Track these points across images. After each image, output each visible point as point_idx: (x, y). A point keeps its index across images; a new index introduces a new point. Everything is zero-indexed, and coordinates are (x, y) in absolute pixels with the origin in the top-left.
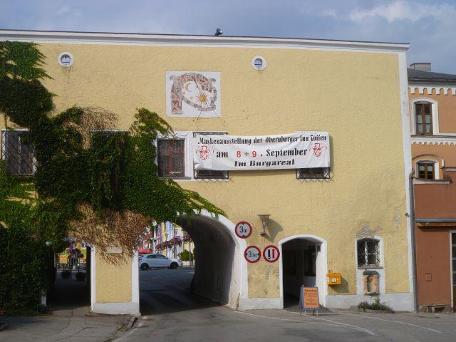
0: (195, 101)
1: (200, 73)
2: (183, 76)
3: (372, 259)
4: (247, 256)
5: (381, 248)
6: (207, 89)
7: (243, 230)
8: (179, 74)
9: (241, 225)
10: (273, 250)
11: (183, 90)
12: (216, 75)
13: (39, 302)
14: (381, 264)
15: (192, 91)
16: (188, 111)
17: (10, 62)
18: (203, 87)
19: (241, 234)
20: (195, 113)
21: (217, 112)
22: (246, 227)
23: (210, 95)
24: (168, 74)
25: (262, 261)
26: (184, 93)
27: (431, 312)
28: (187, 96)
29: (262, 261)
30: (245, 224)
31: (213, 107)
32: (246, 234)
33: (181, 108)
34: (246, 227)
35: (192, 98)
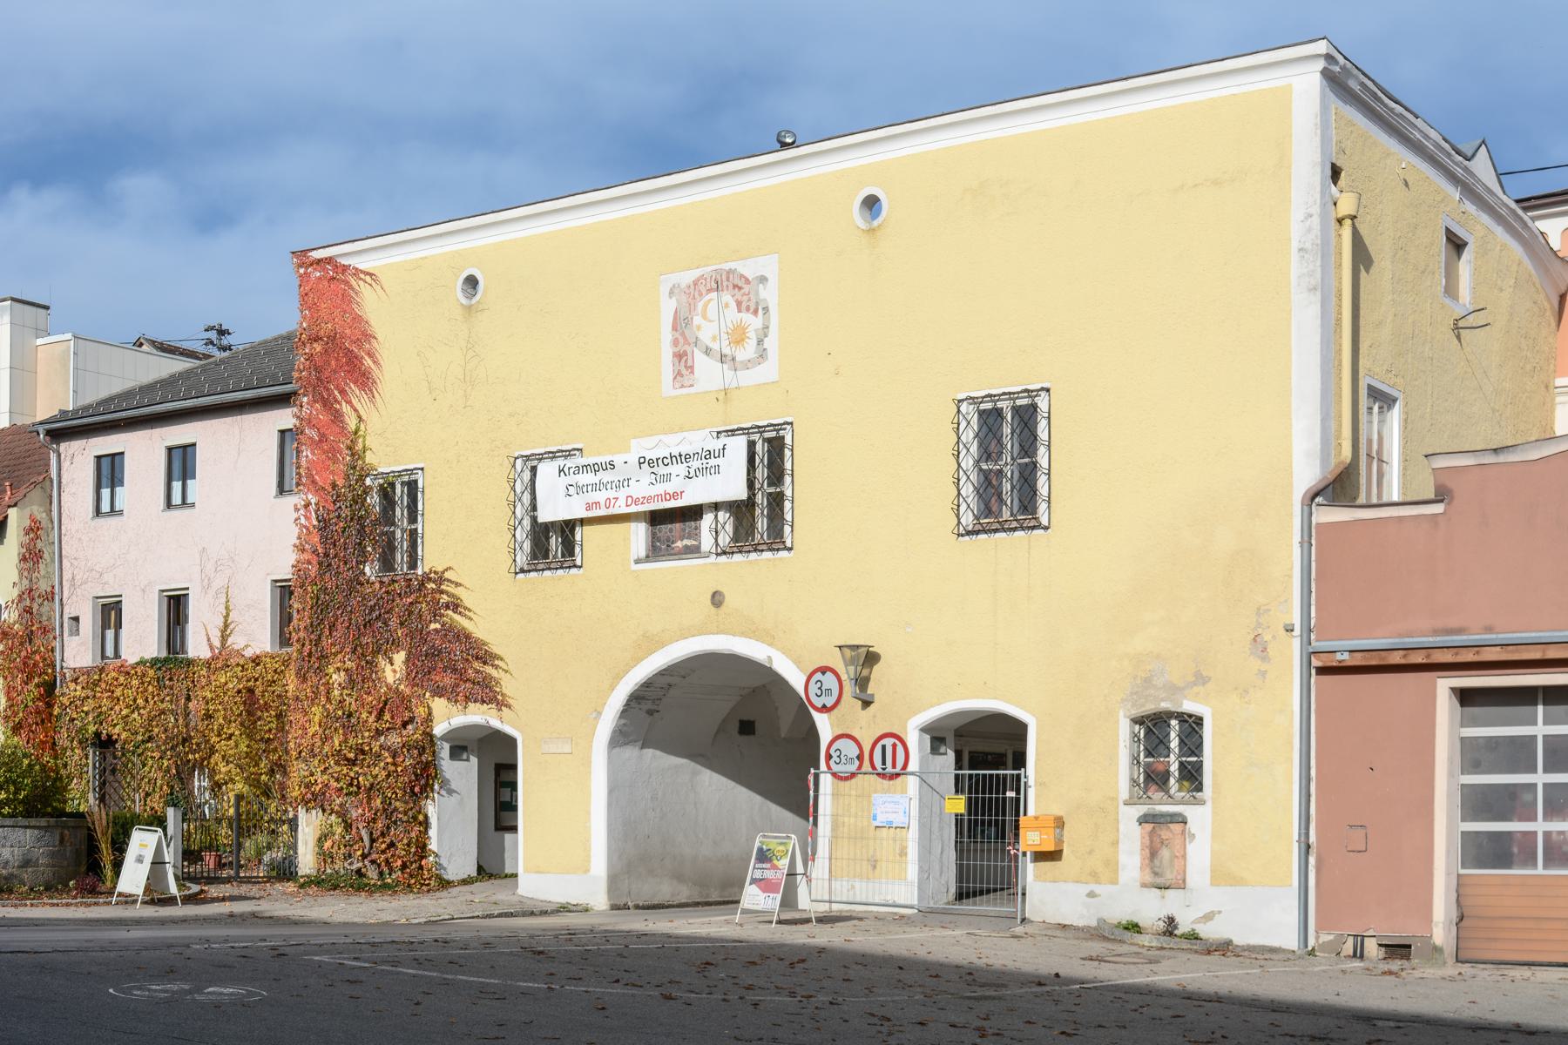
6: (748, 309)
7: (822, 692)
8: (688, 277)
9: (818, 676)
10: (894, 746)
16: (708, 373)
18: (739, 304)
21: (767, 372)
23: (754, 323)
31: (762, 355)
32: (829, 702)
33: (691, 369)
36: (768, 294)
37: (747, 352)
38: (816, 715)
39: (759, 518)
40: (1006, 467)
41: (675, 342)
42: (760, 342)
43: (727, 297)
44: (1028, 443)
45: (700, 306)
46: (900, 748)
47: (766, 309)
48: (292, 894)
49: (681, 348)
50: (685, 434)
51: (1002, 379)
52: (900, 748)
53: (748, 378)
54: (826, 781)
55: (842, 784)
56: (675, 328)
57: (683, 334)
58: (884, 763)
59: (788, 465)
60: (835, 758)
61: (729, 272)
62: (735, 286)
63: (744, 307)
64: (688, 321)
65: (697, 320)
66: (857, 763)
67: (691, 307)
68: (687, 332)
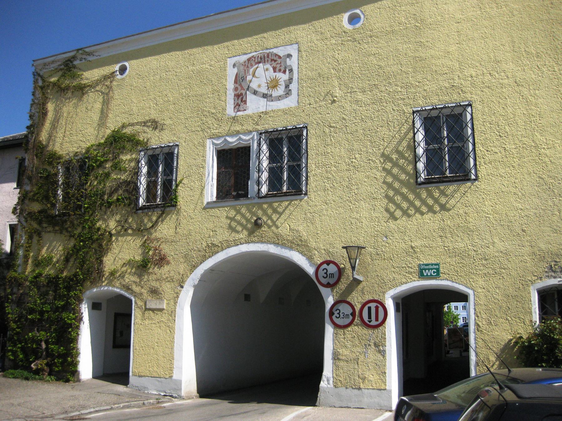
1: (271, 51)
6: (280, 71)
9: (325, 266)
10: (377, 308)
15: (261, 76)
16: (255, 105)
18: (275, 70)
21: (290, 102)
23: (283, 77)
24: (230, 62)
28: (254, 85)
31: (288, 93)
32: (332, 281)
34: (332, 269)
36: (293, 62)
37: (281, 91)
38: (323, 290)
39: (290, 178)
40: (445, 148)
41: (236, 89)
42: (287, 86)
43: (268, 66)
44: (169, 168)
45: (251, 70)
46: (381, 309)
47: (291, 71)
49: (239, 92)
52: (381, 309)
54: (329, 330)
55: (341, 331)
56: (236, 82)
57: (240, 85)
58: (370, 317)
59: (175, 165)
61: (268, 55)
62: (272, 60)
63: (277, 69)
64: (244, 79)
65: (249, 78)
66: (351, 318)
67: (246, 72)
68: (243, 84)
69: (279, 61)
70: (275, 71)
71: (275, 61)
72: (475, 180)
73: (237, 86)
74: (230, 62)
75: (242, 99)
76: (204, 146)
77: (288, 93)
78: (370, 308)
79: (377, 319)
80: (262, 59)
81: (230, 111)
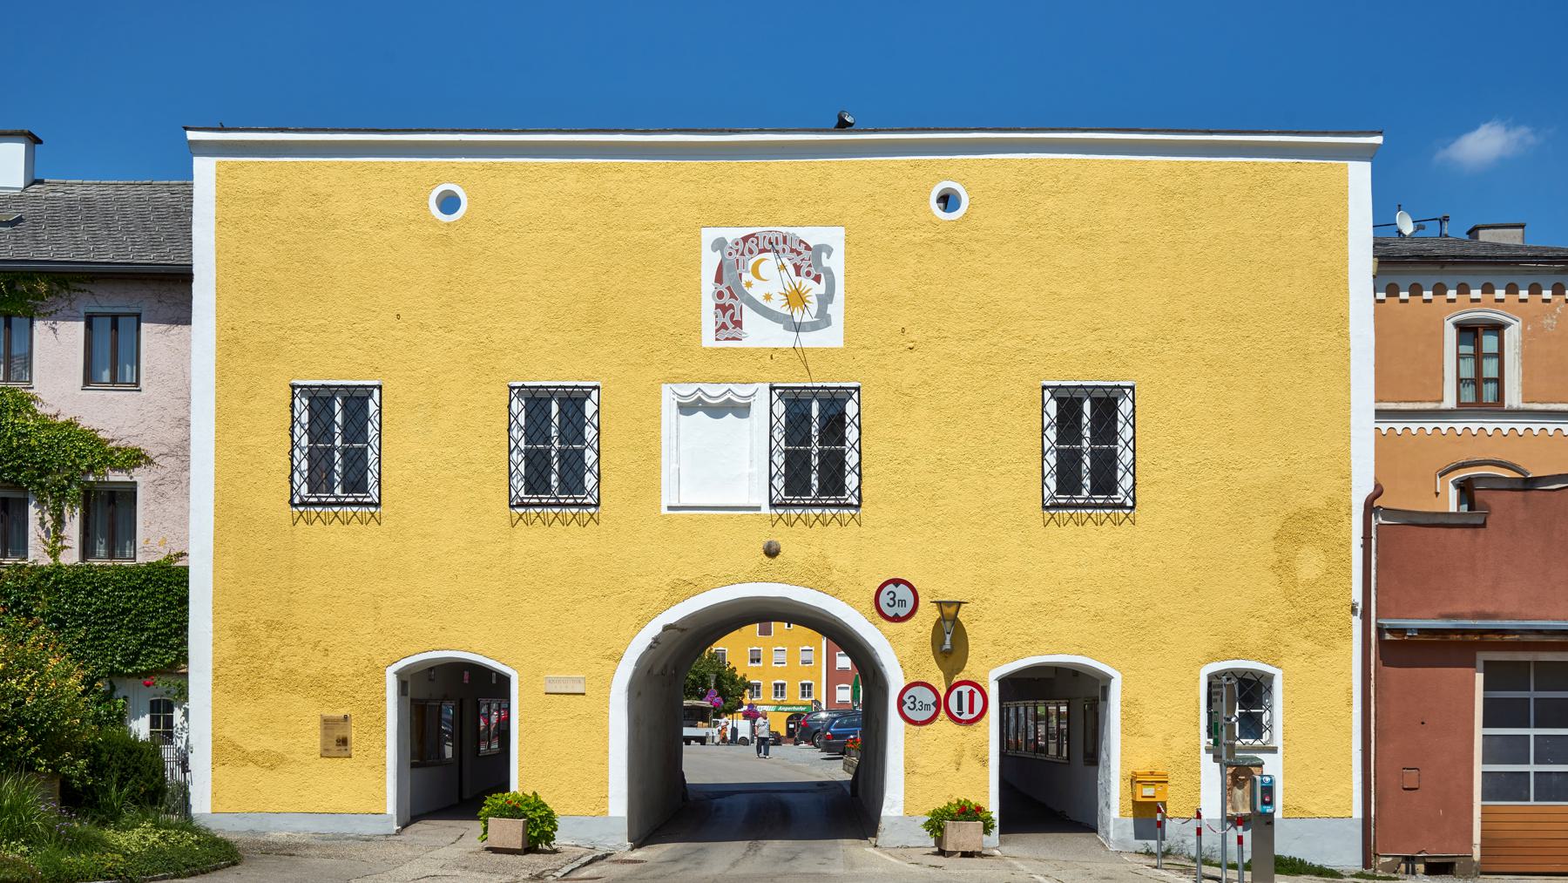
0: (777, 305)
1: (791, 230)
2: (745, 239)
3: (1253, 726)
4: (905, 708)
5: (1278, 712)
6: (808, 274)
7: (894, 602)
8: (733, 234)
9: (891, 587)
10: (972, 693)
11: (747, 277)
12: (832, 236)
13: (441, 754)
14: (1277, 735)
15: (769, 279)
16: (759, 333)
17: (449, 751)
18: (798, 269)
19: (890, 612)
20: (779, 337)
21: (831, 338)
22: (903, 592)
23: (815, 289)
24: (709, 235)
25: (943, 723)
26: (749, 284)
27: (1414, 873)
28: (756, 292)
29: (943, 723)
30: (902, 586)
31: (823, 320)
32: (903, 612)
33: (738, 324)
34: (903, 592)
35: (768, 297)
36: (836, 263)
40: (1087, 445)
46: (978, 696)
48: (186, 714)
50: (731, 386)
51: (1087, 372)
52: (978, 696)
53: (809, 340)
60: (909, 703)
62: (792, 251)
63: (803, 271)
69: (806, 254)
70: (798, 274)
71: (799, 253)
72: (1132, 508)
73: (722, 288)
74: (709, 235)
75: (732, 316)
76: (658, 397)
77: (823, 320)
78: (960, 694)
79: (971, 711)
80: (773, 245)
81: (708, 339)
